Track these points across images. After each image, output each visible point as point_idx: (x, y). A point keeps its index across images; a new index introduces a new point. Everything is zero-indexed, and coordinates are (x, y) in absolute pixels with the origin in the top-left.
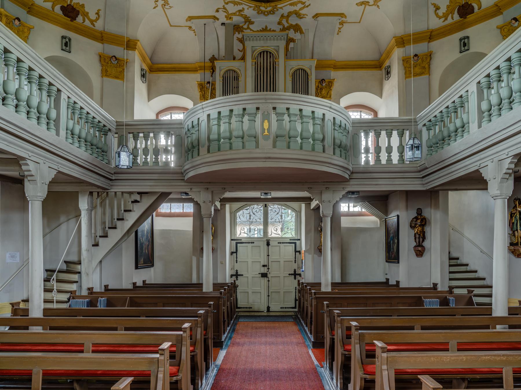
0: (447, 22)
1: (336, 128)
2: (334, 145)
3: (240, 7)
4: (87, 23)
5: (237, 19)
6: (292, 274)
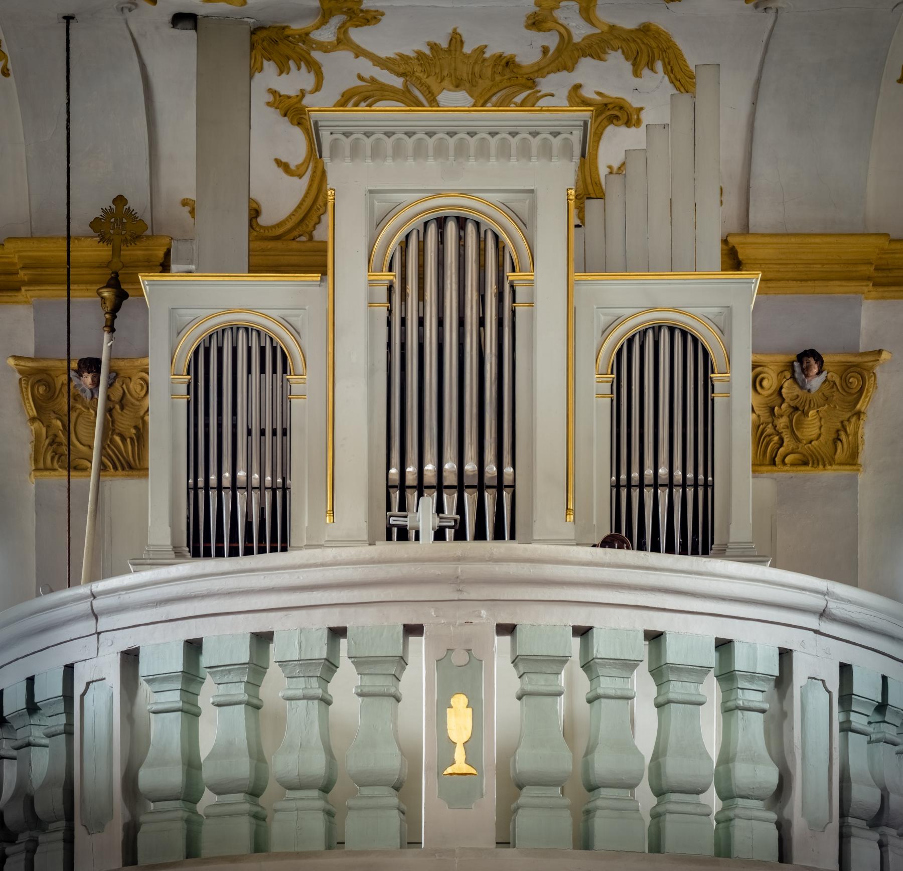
1: (858, 721)
2: (843, 815)
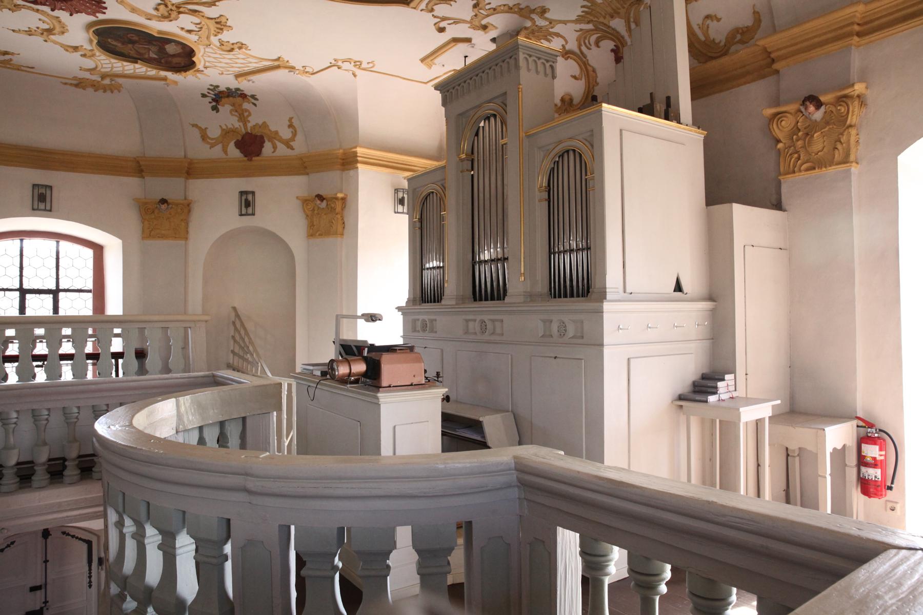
4: (282, 150)
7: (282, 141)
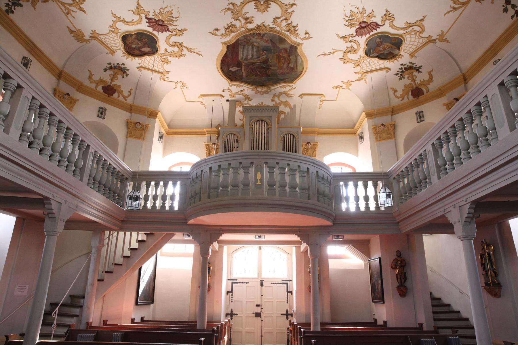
0: (404, 101)
3: (241, 89)
5: (237, 97)
6: (284, 314)
7: (123, 95)
